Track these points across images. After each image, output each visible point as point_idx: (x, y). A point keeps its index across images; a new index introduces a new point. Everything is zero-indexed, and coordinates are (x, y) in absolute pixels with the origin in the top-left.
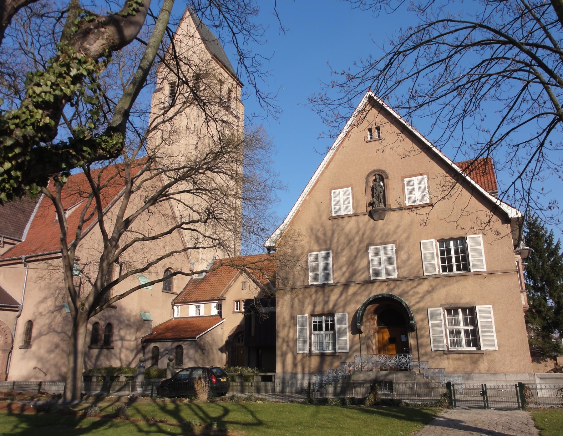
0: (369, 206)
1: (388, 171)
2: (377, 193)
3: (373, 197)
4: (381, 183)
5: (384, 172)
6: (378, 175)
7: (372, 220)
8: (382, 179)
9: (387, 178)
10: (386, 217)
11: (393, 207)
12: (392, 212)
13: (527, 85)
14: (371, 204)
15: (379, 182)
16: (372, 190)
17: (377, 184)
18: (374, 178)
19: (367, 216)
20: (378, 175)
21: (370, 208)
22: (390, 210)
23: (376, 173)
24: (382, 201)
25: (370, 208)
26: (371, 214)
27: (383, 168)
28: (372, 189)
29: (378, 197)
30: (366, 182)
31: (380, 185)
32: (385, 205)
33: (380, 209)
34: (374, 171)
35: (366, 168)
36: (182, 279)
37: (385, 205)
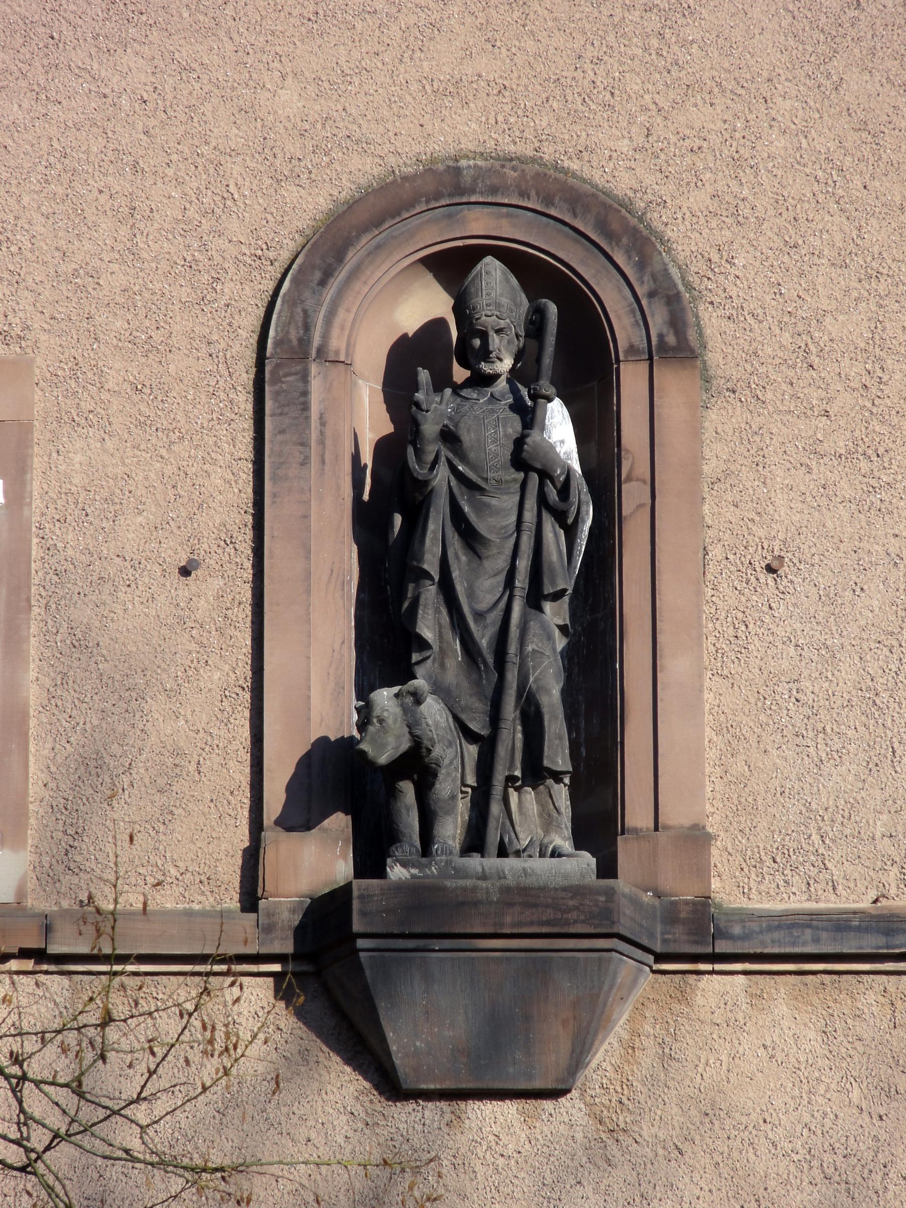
0: (301, 816)
1: (688, 237)
2: (481, 588)
3: (385, 648)
4: (559, 428)
5: (617, 228)
6: (525, 266)
7: (342, 1086)
8: (579, 356)
9: (677, 347)
10: (605, 1056)
11: (736, 886)
12: (718, 991)
13: (109, 1116)
14: (347, 784)
15: (529, 416)
16: (368, 521)
17: (489, 430)
18: (424, 304)
19: (252, 1001)
20: (525, 266)
21: (318, 860)
22: (700, 940)
23: (478, 224)
24: (557, 755)
25: (318, 860)
26: (333, 972)
27: (611, 160)
28: (392, 509)
29: (490, 662)
30: (279, 365)
31: (525, 459)
32: (598, 827)
33: (525, 895)
34: (450, 184)
35: (289, 101)
36: (662, 700)
37: (598, 827)
